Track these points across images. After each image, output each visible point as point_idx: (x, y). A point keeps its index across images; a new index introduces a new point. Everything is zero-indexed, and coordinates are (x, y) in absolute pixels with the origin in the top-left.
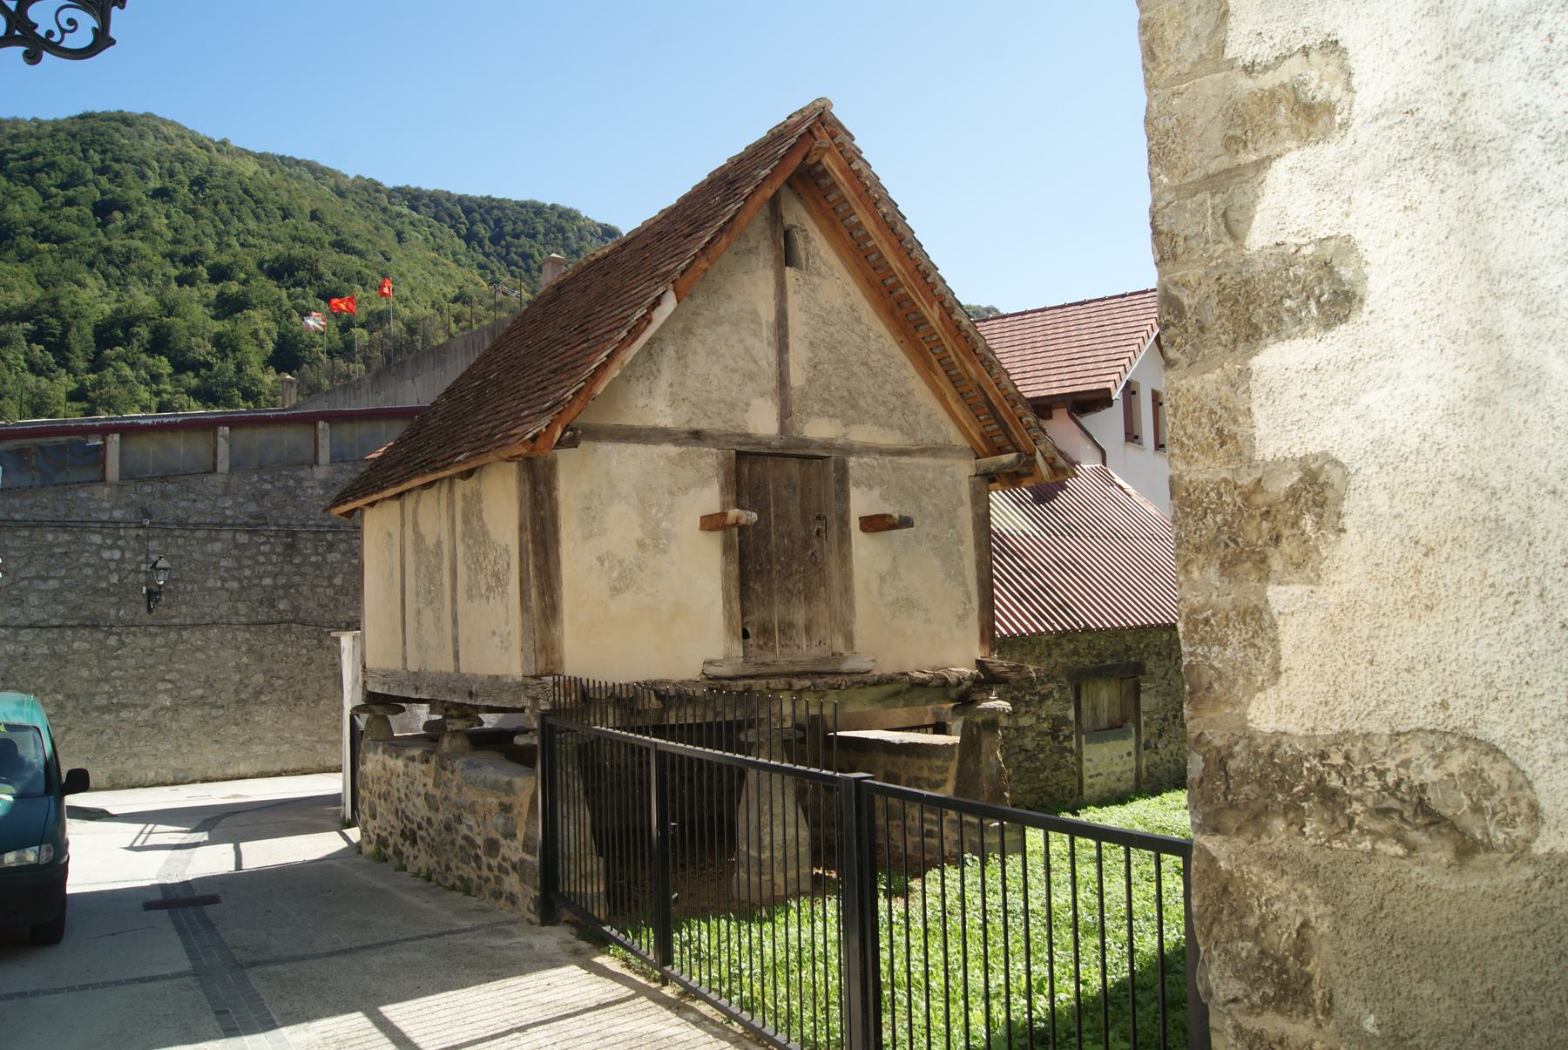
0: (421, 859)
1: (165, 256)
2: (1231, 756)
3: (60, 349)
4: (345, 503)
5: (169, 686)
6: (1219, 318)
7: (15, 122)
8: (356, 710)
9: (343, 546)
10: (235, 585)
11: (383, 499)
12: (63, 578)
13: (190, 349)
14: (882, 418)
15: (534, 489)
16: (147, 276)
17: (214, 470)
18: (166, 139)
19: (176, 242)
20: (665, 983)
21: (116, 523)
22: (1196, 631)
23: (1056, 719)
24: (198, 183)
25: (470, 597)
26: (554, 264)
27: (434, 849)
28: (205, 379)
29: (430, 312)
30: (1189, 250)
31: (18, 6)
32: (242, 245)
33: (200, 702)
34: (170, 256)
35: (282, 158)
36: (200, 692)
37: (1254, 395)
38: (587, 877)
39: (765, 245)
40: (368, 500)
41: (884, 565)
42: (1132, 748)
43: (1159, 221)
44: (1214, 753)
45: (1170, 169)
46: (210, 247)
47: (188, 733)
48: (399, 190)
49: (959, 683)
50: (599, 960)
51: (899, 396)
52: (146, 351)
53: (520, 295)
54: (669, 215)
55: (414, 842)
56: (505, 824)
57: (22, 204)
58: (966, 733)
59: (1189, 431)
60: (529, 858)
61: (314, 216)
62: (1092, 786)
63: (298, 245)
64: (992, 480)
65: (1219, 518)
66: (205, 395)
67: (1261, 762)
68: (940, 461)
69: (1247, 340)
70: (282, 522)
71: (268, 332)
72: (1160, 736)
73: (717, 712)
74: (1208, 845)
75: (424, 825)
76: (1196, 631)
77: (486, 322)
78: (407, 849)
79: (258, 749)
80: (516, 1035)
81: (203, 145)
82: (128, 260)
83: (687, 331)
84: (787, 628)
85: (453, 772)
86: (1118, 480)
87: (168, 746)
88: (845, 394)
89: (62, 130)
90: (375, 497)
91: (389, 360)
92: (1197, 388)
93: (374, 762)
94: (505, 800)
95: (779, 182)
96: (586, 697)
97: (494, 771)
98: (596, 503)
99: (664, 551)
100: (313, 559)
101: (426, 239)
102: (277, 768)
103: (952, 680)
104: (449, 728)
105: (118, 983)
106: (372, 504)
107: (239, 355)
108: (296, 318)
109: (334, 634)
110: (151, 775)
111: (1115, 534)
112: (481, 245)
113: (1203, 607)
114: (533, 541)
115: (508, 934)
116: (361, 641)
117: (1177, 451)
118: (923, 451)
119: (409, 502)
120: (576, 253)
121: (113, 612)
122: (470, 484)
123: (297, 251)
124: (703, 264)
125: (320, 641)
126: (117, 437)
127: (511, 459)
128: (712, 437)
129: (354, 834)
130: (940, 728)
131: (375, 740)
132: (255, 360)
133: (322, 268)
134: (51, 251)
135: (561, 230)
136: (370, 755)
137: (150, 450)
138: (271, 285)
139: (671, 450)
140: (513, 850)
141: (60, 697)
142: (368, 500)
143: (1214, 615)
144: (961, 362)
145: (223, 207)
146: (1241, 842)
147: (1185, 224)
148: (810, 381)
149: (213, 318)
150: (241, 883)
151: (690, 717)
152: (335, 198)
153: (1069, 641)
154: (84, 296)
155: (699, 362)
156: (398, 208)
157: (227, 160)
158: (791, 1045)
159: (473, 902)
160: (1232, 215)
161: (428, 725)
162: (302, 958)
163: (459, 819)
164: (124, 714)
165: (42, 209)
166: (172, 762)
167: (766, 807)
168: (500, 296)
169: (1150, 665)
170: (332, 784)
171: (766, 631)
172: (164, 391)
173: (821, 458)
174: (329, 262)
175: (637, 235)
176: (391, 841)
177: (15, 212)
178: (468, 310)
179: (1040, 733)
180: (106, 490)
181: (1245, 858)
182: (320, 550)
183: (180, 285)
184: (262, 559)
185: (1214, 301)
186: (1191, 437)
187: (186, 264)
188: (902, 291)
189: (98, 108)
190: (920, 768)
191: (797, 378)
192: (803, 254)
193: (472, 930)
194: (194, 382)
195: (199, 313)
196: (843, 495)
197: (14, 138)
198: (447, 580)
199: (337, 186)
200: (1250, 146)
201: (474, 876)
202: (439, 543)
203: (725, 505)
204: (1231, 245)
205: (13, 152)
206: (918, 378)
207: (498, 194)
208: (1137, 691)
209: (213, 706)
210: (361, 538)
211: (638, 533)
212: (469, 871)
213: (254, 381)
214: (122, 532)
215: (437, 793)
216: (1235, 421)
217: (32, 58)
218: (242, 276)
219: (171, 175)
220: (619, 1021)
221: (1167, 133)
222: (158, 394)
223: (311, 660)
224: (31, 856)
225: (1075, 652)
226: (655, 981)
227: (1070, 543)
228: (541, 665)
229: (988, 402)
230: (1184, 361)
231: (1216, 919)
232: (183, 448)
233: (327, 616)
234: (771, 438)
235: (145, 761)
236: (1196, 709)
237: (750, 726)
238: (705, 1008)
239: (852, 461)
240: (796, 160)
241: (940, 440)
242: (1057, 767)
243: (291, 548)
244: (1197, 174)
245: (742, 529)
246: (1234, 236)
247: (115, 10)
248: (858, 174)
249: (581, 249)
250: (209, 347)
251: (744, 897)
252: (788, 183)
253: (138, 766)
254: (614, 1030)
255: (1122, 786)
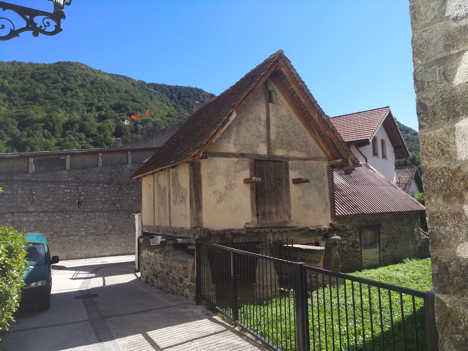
0: (159, 283)
1: (83, 104)
2: (450, 266)
3: (53, 131)
4: (136, 176)
5: (84, 229)
6: (442, 110)
7: (38, 64)
8: (140, 237)
9: (136, 188)
10: (104, 199)
11: (148, 174)
12: (53, 198)
13: (90, 131)
14: (299, 148)
15: (194, 171)
16: (78, 110)
17: (97, 166)
18: (83, 70)
19: (86, 100)
20: (236, 326)
21: (69, 182)
22: (434, 221)
23: (353, 241)
24: (92, 83)
25: (174, 204)
26: (197, 106)
27: (163, 280)
28: (95, 139)
29: (160, 119)
30: (430, 87)
31: (30, 18)
32: (105, 100)
33: (93, 234)
34: (85, 104)
35: (117, 75)
36: (94, 231)
37: (457, 137)
38: (210, 290)
39: (263, 96)
40: (144, 175)
41: (300, 194)
42: (378, 251)
43: (417, 76)
44: (442, 265)
45: (421, 59)
46: (96, 101)
47: (90, 243)
48: (150, 84)
49: (325, 230)
50: (214, 317)
51: (304, 142)
52: (78, 131)
53: (186, 114)
54: (233, 88)
55: (157, 278)
56: (185, 273)
57: (40, 89)
58: (326, 246)
59: (430, 150)
60: (192, 284)
61: (126, 92)
62: (365, 262)
63: (121, 100)
64: (334, 168)
65: (442, 181)
66: (95, 144)
67: (463, 269)
68: (317, 162)
69: (454, 117)
70: (117, 181)
71: (113, 126)
72: (387, 247)
73: (247, 239)
74: (441, 298)
75: (160, 273)
76: (434, 221)
77: (176, 123)
78: (155, 280)
79: (110, 248)
80: (189, 343)
81: (94, 71)
82: (72, 105)
83: (240, 123)
84: (270, 213)
85: (169, 257)
86: (371, 167)
87: (84, 247)
88: (288, 142)
89: (52, 67)
90: (145, 174)
91: (149, 134)
92: (433, 135)
93: (145, 253)
94: (185, 266)
95: (267, 76)
96: (210, 234)
97: (182, 257)
98: (213, 175)
99: (233, 190)
100: (127, 192)
101: (159, 98)
102: (116, 254)
103: (323, 230)
104: (168, 243)
105: (65, 324)
106: (145, 176)
107: (105, 132)
108: (121, 122)
109: (133, 214)
110: (79, 255)
111: (371, 184)
112: (175, 100)
113: (436, 212)
114: (194, 187)
115: (186, 308)
116: (141, 216)
117: (425, 157)
118: (312, 159)
119: (156, 175)
120: (202, 102)
121: (68, 208)
122: (174, 170)
123: (121, 102)
124: (245, 102)
125: (129, 216)
126: (69, 156)
127: (187, 162)
128: (247, 155)
129: (139, 274)
130: (317, 244)
131: (145, 247)
132: (109, 134)
133: (129, 107)
134: (50, 103)
135: (198, 95)
136: (144, 251)
137: (79, 159)
138: (114, 112)
139: (235, 159)
140: (187, 281)
141: (52, 233)
142: (144, 175)
143: (441, 215)
144: (324, 131)
145: (100, 89)
146: (455, 298)
147: (428, 77)
148: (277, 138)
149: (97, 122)
150: (104, 289)
151: (241, 240)
152: (132, 86)
153: (358, 217)
154: (60, 115)
155: (243, 133)
156: (150, 89)
157: (101, 76)
158: (278, 350)
159: (175, 297)
160: (447, 73)
161: (161, 242)
162: (123, 315)
163: (171, 271)
164: (71, 238)
165: (46, 90)
166: (85, 252)
167: (265, 269)
168: (181, 115)
169: (383, 225)
170: (132, 258)
171: (264, 214)
172: (83, 143)
173: (280, 161)
174: (130, 105)
175: (219, 97)
176: (150, 277)
177: (38, 91)
178: (171, 119)
179: (348, 246)
180: (66, 172)
181: (457, 304)
182: (129, 189)
183: (88, 112)
184: (112, 192)
185: (440, 104)
186: (430, 152)
187: (89, 106)
188: (305, 109)
189: (62, 61)
190: (312, 257)
191: (273, 137)
192: (274, 99)
193: (175, 306)
194: (92, 140)
195: (93, 120)
196: (287, 173)
197: (37, 69)
198: (167, 199)
199: (133, 83)
200: (455, 47)
201: (175, 289)
202: (165, 188)
203: (251, 176)
204: (447, 84)
205: (37, 73)
206: (310, 136)
207: (179, 85)
208: (379, 233)
209: (97, 235)
210: (141, 186)
211: (225, 184)
212: (174, 287)
213: (109, 140)
214: (71, 184)
215: (164, 263)
216: (449, 146)
217: (36, 34)
218: (105, 109)
219: (84, 80)
220: (222, 338)
221: (421, 45)
222: (81, 144)
223: (126, 222)
224: (40, 284)
225: (359, 221)
226: (233, 325)
227: (357, 187)
228: (196, 224)
229: (333, 143)
230: (427, 125)
231: (446, 325)
232: (88, 159)
233: (131, 209)
234: (265, 155)
235: (77, 251)
236: (434, 248)
237: (259, 243)
238: (249, 335)
239: (290, 162)
240: (273, 69)
241: (317, 155)
242: (354, 257)
243: (120, 189)
244: (433, 59)
245: (256, 183)
246: (447, 80)
247: (62, 19)
248: (292, 73)
249: (204, 101)
250: (96, 130)
251: (258, 296)
252: (270, 77)
253: (75, 253)
254: (220, 342)
255: (375, 263)
